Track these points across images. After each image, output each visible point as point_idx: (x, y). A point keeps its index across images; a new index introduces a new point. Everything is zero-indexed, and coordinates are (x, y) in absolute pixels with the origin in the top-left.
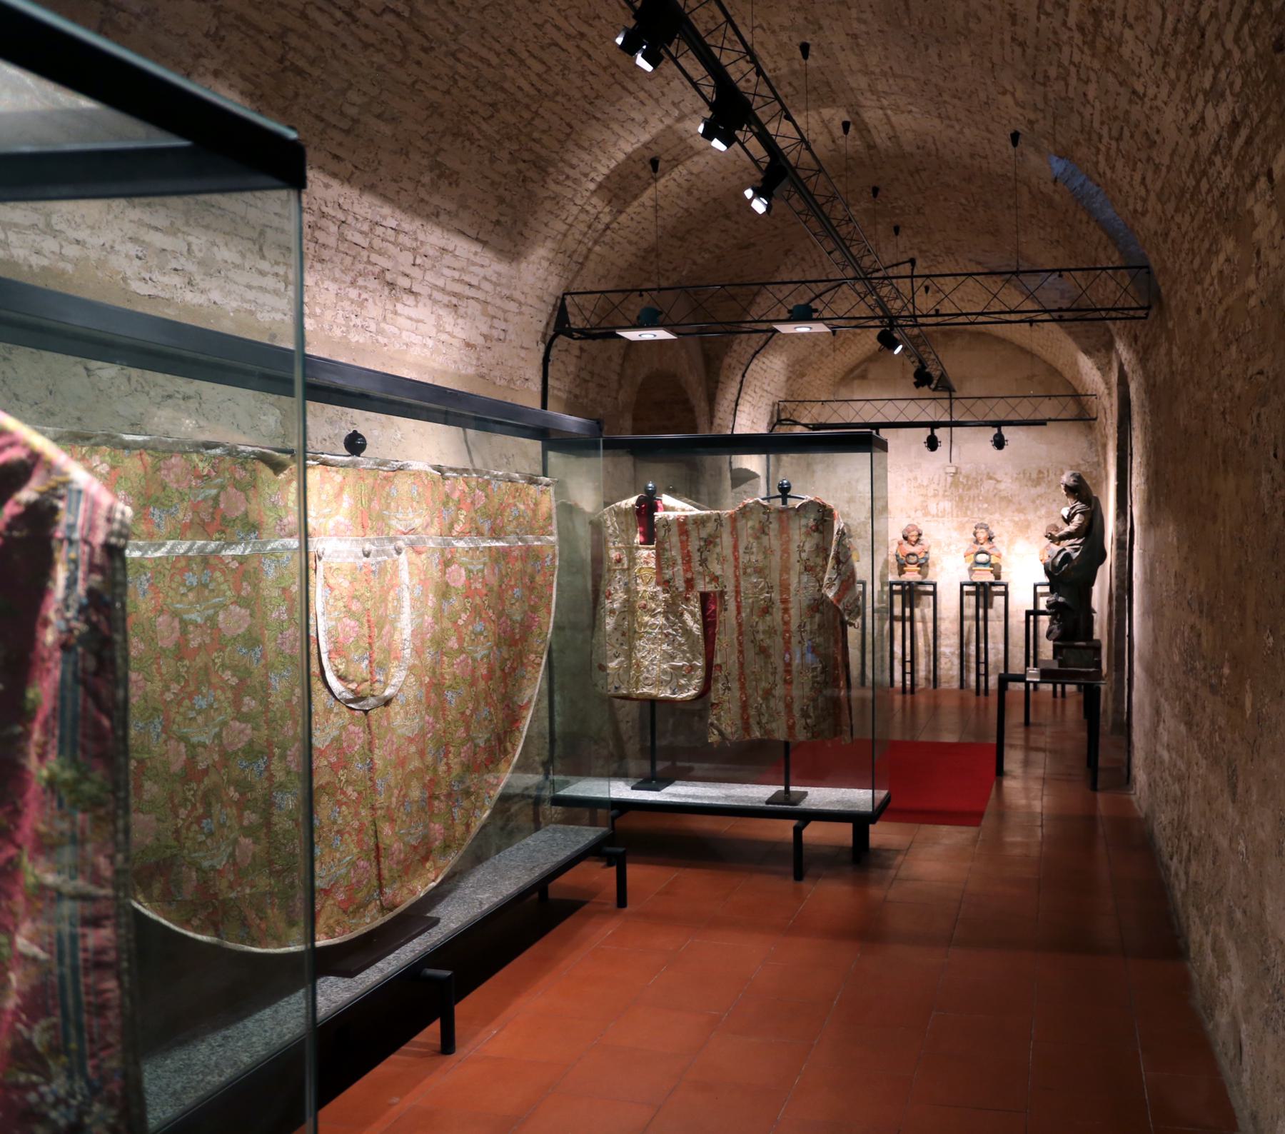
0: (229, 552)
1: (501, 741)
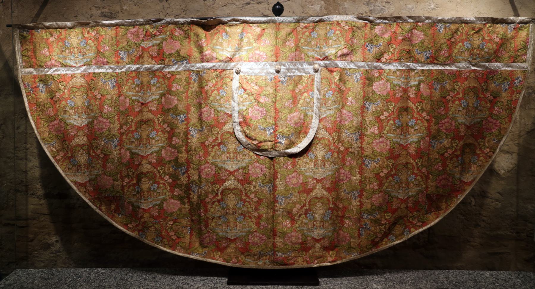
0: (167, 70)
1: (440, 197)
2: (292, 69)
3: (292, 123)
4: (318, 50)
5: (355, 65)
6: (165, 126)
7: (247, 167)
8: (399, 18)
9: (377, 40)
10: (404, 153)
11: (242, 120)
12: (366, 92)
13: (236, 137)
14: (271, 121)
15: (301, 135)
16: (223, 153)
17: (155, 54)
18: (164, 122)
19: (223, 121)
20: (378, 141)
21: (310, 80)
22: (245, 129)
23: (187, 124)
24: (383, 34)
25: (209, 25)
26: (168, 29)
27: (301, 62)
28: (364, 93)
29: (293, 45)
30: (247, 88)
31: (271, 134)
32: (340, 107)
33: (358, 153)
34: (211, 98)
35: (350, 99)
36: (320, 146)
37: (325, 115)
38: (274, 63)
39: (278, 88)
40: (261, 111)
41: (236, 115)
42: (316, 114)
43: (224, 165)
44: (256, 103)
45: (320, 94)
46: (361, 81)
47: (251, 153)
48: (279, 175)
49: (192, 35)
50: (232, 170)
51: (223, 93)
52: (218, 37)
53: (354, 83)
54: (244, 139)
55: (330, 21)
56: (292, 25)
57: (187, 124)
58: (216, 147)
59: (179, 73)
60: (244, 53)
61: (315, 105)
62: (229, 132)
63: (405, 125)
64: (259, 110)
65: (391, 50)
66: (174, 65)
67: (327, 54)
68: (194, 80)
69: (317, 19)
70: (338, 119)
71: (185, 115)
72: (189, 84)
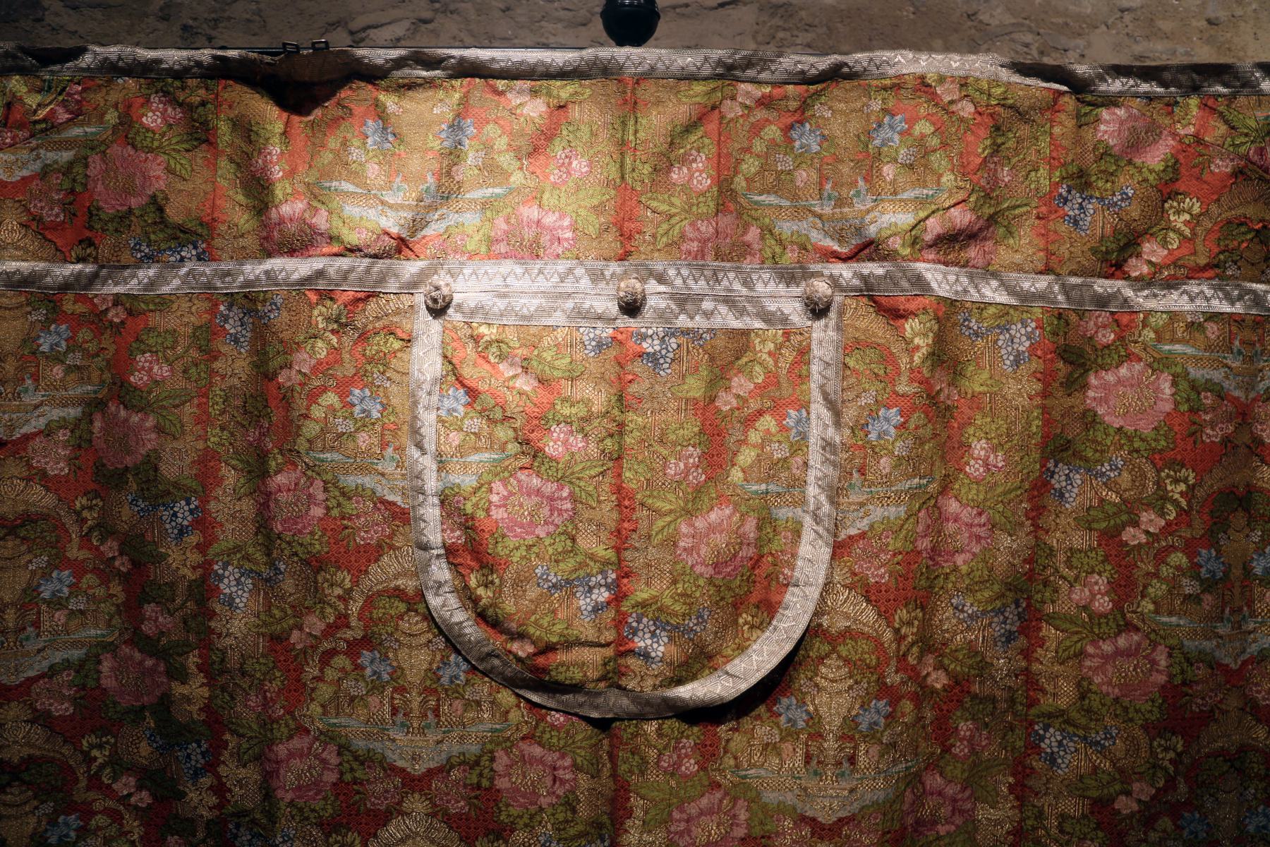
2: (700, 298)
3: (700, 561)
4: (827, 210)
5: (1006, 287)
6: (110, 548)
7: (485, 761)
8: (1218, 72)
9: (1110, 176)
10: (1233, 702)
11: (457, 537)
12: (1056, 415)
13: (429, 617)
14: (595, 545)
15: (745, 617)
16: (376, 687)
17: (54, 214)
18: (105, 529)
19: (373, 537)
20: (1107, 647)
21: (789, 355)
22: (473, 582)
23: (202, 548)
24: (1135, 144)
25: (309, 83)
26: (114, 97)
27: (747, 265)
28: (1047, 422)
29: (703, 181)
30: (482, 387)
31: (596, 609)
32: (933, 488)
33: (1012, 701)
34: (311, 429)
35: (979, 447)
36: (831, 670)
37: (863, 525)
38: (614, 267)
39: (633, 389)
40: (551, 499)
41: (431, 512)
42: (817, 519)
43: (377, 746)
44: (525, 461)
45: (838, 424)
46: (1036, 365)
47: (506, 697)
48: (636, 802)
49: (224, 128)
50: (419, 769)
51: (368, 405)
52: (345, 143)
53: (1004, 376)
54: (472, 631)
55: (883, 76)
56: (699, 88)
57: (202, 548)
58: (341, 661)
59: (163, 303)
60: (465, 221)
61: (812, 476)
62: (399, 593)
63: (1237, 572)
64: (538, 492)
65: (1179, 221)
66: (139, 264)
67: (872, 231)
68: (236, 341)
69: (824, 63)
70: (924, 544)
71: (195, 503)
72: (214, 356)
